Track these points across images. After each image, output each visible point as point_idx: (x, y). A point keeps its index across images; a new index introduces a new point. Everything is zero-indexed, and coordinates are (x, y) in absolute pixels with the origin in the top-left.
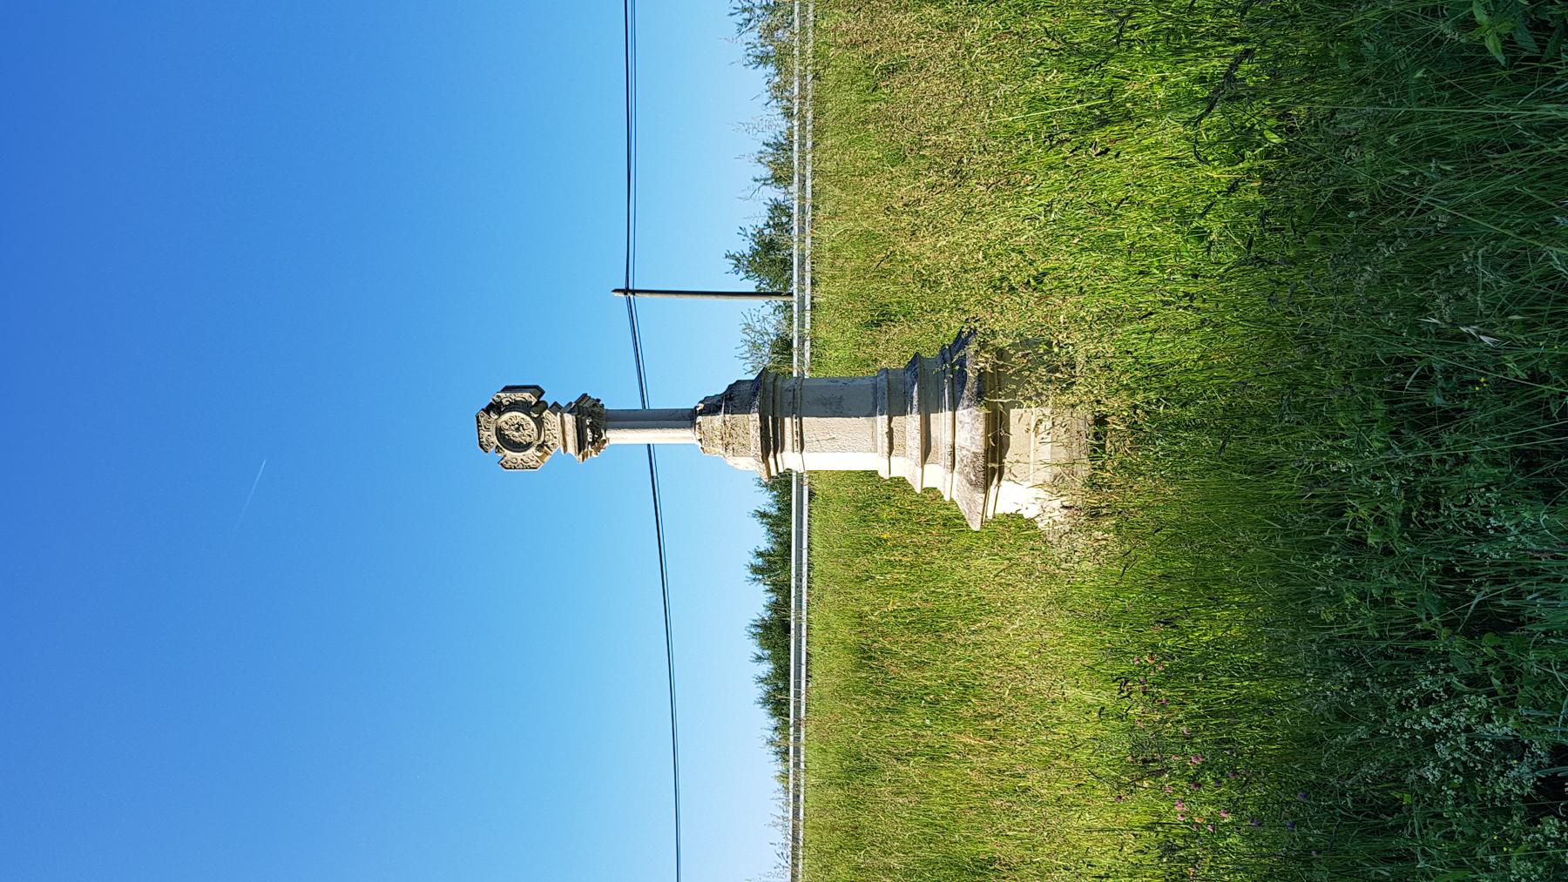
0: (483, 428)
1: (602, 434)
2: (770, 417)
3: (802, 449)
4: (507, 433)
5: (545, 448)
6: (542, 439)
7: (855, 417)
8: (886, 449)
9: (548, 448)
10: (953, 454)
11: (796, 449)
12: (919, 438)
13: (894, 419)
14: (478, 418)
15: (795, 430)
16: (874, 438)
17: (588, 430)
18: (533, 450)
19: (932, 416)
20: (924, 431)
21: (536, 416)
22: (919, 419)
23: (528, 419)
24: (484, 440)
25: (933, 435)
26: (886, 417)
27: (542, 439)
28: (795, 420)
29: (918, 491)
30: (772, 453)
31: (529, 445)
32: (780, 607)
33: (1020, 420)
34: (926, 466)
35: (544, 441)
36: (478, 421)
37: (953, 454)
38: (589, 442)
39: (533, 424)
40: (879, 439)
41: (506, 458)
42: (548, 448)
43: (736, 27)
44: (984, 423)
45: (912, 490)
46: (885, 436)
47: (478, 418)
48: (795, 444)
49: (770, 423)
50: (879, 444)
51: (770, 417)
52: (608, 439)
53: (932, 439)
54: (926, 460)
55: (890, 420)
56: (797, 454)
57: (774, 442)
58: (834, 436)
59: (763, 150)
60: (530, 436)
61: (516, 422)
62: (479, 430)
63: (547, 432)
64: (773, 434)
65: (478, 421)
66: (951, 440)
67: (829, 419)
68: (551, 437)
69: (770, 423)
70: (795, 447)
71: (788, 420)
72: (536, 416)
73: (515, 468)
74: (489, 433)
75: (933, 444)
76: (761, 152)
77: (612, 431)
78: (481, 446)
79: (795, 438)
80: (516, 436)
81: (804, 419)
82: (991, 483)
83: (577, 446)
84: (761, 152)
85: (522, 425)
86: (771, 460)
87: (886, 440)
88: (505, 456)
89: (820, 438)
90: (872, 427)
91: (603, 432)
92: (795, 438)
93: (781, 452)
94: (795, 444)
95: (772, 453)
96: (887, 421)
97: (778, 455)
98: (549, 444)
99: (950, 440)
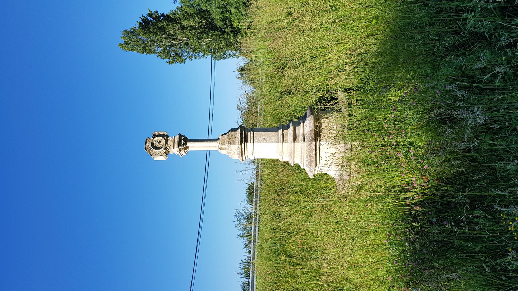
0: (147, 143)
1: (187, 143)
2: (243, 131)
3: (253, 142)
4: (155, 144)
5: (167, 149)
6: (166, 146)
7: (271, 132)
8: (282, 140)
9: (168, 149)
10: (304, 136)
11: (251, 142)
12: (293, 133)
13: (284, 131)
14: (146, 140)
15: (251, 135)
16: (278, 138)
17: (183, 140)
18: (162, 149)
19: (297, 127)
20: (294, 131)
21: (166, 138)
22: (292, 127)
23: (163, 139)
24: (146, 147)
25: (297, 133)
26: (281, 129)
27: (166, 146)
28: (251, 132)
29: (293, 165)
30: (243, 142)
31: (161, 148)
32: (242, 278)
33: (325, 122)
34: (295, 143)
35: (167, 147)
36: (146, 141)
37: (304, 136)
38: (182, 145)
39: (164, 141)
40: (279, 137)
41: (153, 153)
42: (168, 149)
43: (235, 225)
44: (313, 120)
45: (291, 165)
46: (281, 135)
47: (146, 140)
48: (251, 140)
49: (243, 133)
50: (279, 139)
51: (243, 131)
52: (189, 147)
53: (297, 135)
54: (295, 141)
55: (283, 131)
56: (252, 143)
57: (244, 139)
58: (265, 138)
59: (241, 263)
60: (162, 145)
61: (159, 141)
62: (146, 144)
63: (168, 144)
64: (244, 136)
65: (146, 141)
66: (303, 132)
67: (263, 132)
68: (170, 145)
69: (243, 133)
70: (251, 141)
71: (249, 133)
72: (166, 138)
73: (155, 156)
74: (149, 145)
75: (297, 136)
76: (241, 264)
77: (190, 142)
78: (145, 149)
79: (251, 138)
80: (158, 145)
81: (255, 133)
82: (317, 141)
83: (178, 144)
84: (241, 264)
85: (161, 142)
86: (243, 145)
87: (282, 137)
88: (153, 152)
89: (259, 139)
90: (277, 135)
91: (187, 142)
92: (251, 138)
93: (247, 143)
94: (251, 140)
95: (243, 142)
96: (282, 131)
97: (245, 144)
98: (168, 148)
99: (302, 132)
